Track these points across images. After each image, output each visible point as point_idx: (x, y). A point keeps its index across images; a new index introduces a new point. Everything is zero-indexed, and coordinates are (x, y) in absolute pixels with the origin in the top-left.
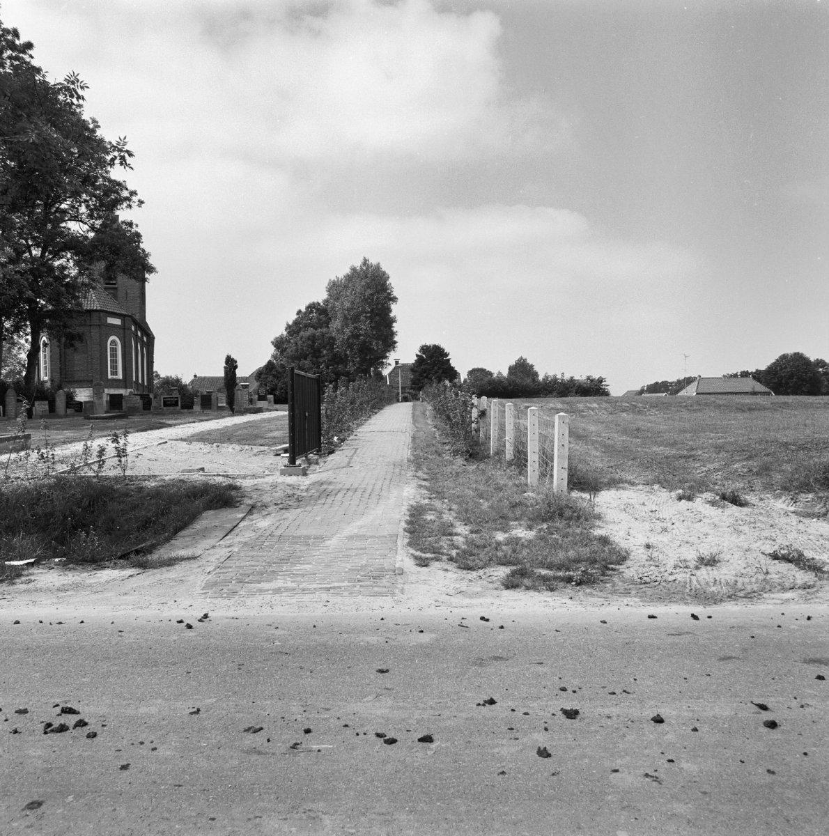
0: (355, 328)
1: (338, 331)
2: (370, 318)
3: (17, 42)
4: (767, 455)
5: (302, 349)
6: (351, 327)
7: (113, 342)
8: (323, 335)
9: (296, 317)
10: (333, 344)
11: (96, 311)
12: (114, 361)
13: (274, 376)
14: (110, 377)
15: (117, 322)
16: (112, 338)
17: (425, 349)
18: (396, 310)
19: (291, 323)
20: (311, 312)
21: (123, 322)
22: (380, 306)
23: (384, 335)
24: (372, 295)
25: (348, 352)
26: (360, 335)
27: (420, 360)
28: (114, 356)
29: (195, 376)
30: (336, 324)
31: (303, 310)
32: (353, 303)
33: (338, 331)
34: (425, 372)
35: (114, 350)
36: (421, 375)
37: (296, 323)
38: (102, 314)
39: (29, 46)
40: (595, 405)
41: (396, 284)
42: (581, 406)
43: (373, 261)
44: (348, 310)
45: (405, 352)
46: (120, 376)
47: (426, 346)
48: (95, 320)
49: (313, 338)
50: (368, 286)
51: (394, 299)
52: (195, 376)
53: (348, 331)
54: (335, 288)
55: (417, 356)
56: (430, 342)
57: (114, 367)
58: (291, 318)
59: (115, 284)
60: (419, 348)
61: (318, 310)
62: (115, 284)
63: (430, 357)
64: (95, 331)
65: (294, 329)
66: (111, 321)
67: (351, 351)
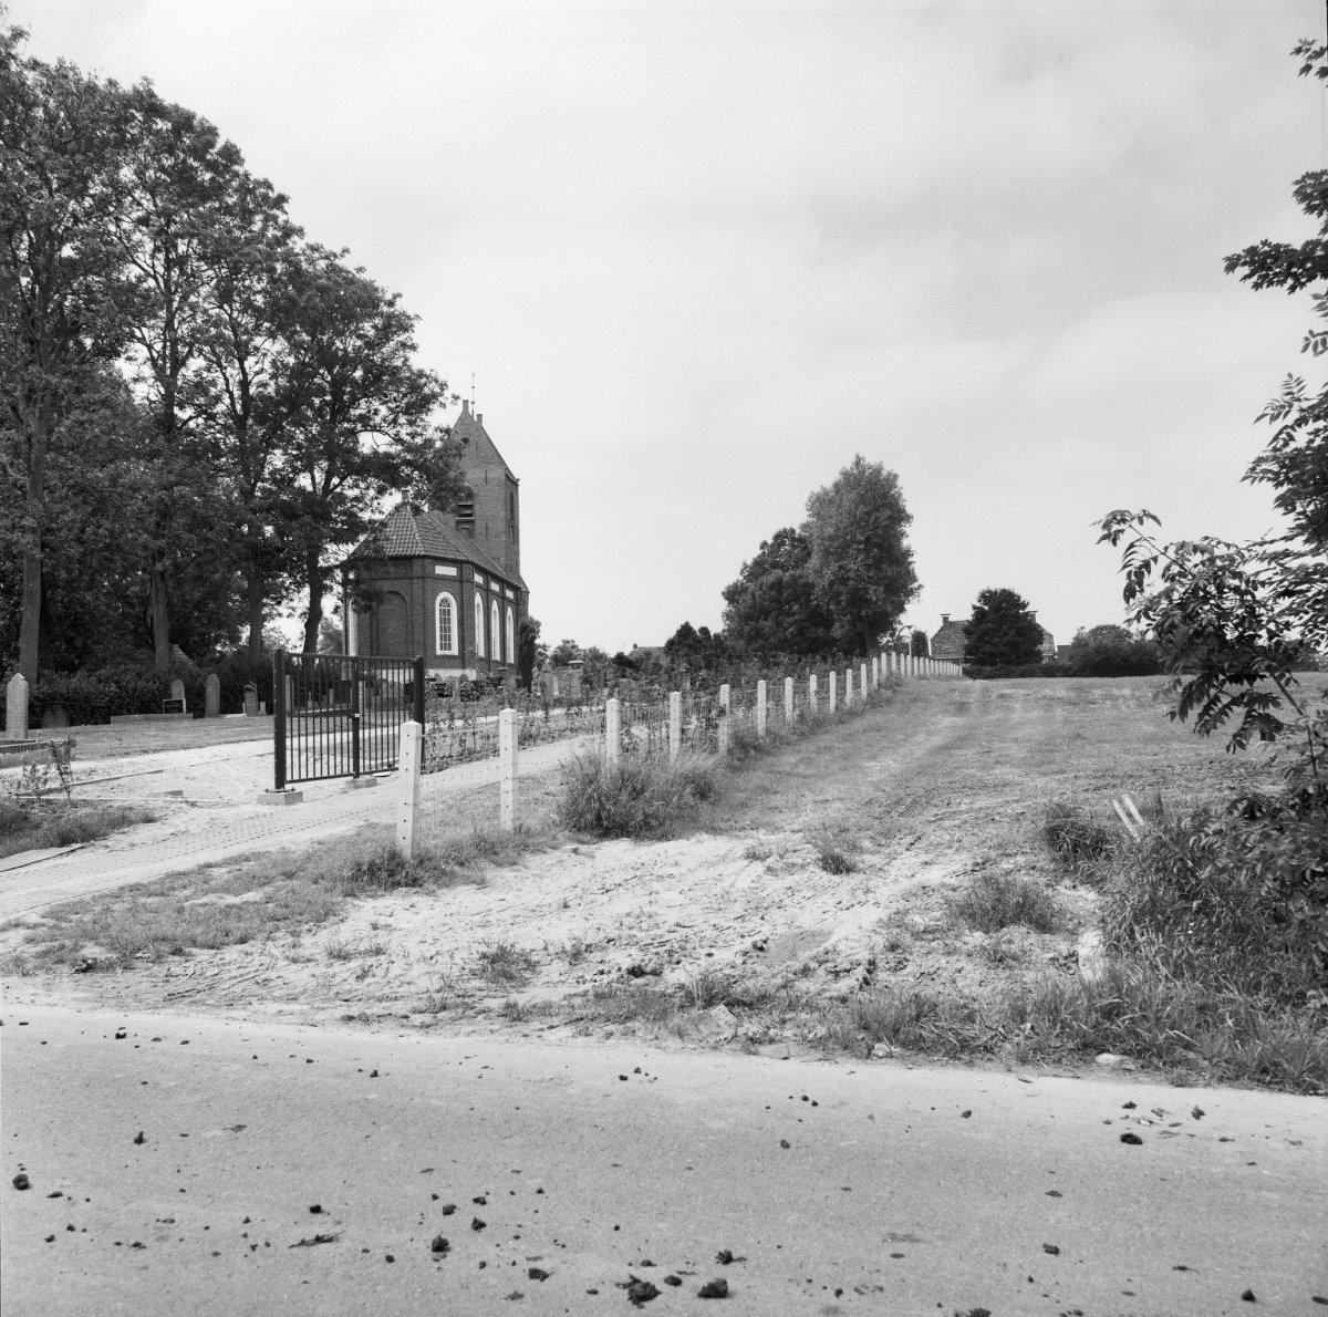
0: (841, 568)
1: (816, 572)
2: (864, 550)
3: (271, 194)
4: (1113, 776)
5: (761, 604)
6: (834, 567)
7: (444, 601)
8: (794, 579)
9: (759, 552)
10: (809, 594)
11: (419, 557)
12: (446, 629)
13: (690, 646)
14: (439, 652)
15: (452, 571)
16: (443, 595)
17: (987, 597)
18: (914, 537)
19: (749, 562)
20: (783, 544)
21: (460, 571)
22: (880, 532)
23: (896, 579)
24: (869, 514)
25: (832, 607)
26: (848, 579)
27: (979, 613)
28: (446, 621)
29: (635, 646)
30: (815, 561)
31: (770, 541)
32: (837, 528)
33: (816, 572)
34: (987, 634)
35: (446, 613)
36: (980, 640)
37: (758, 563)
38: (427, 561)
39: (282, 199)
40: (1127, 692)
41: (911, 497)
42: (1097, 693)
43: (871, 460)
44: (831, 538)
45: (939, 599)
46: (455, 651)
47: (990, 592)
48: (417, 569)
49: (778, 585)
50: (862, 500)
51: (908, 518)
52: (635, 646)
53: (828, 574)
54: (820, 504)
55: (974, 607)
56: (996, 585)
57: (446, 638)
58: (752, 553)
59: (471, 515)
60: (977, 595)
61: (793, 539)
62: (471, 515)
63: (996, 609)
64: (417, 584)
65: (757, 569)
66: (440, 570)
67: (838, 603)
